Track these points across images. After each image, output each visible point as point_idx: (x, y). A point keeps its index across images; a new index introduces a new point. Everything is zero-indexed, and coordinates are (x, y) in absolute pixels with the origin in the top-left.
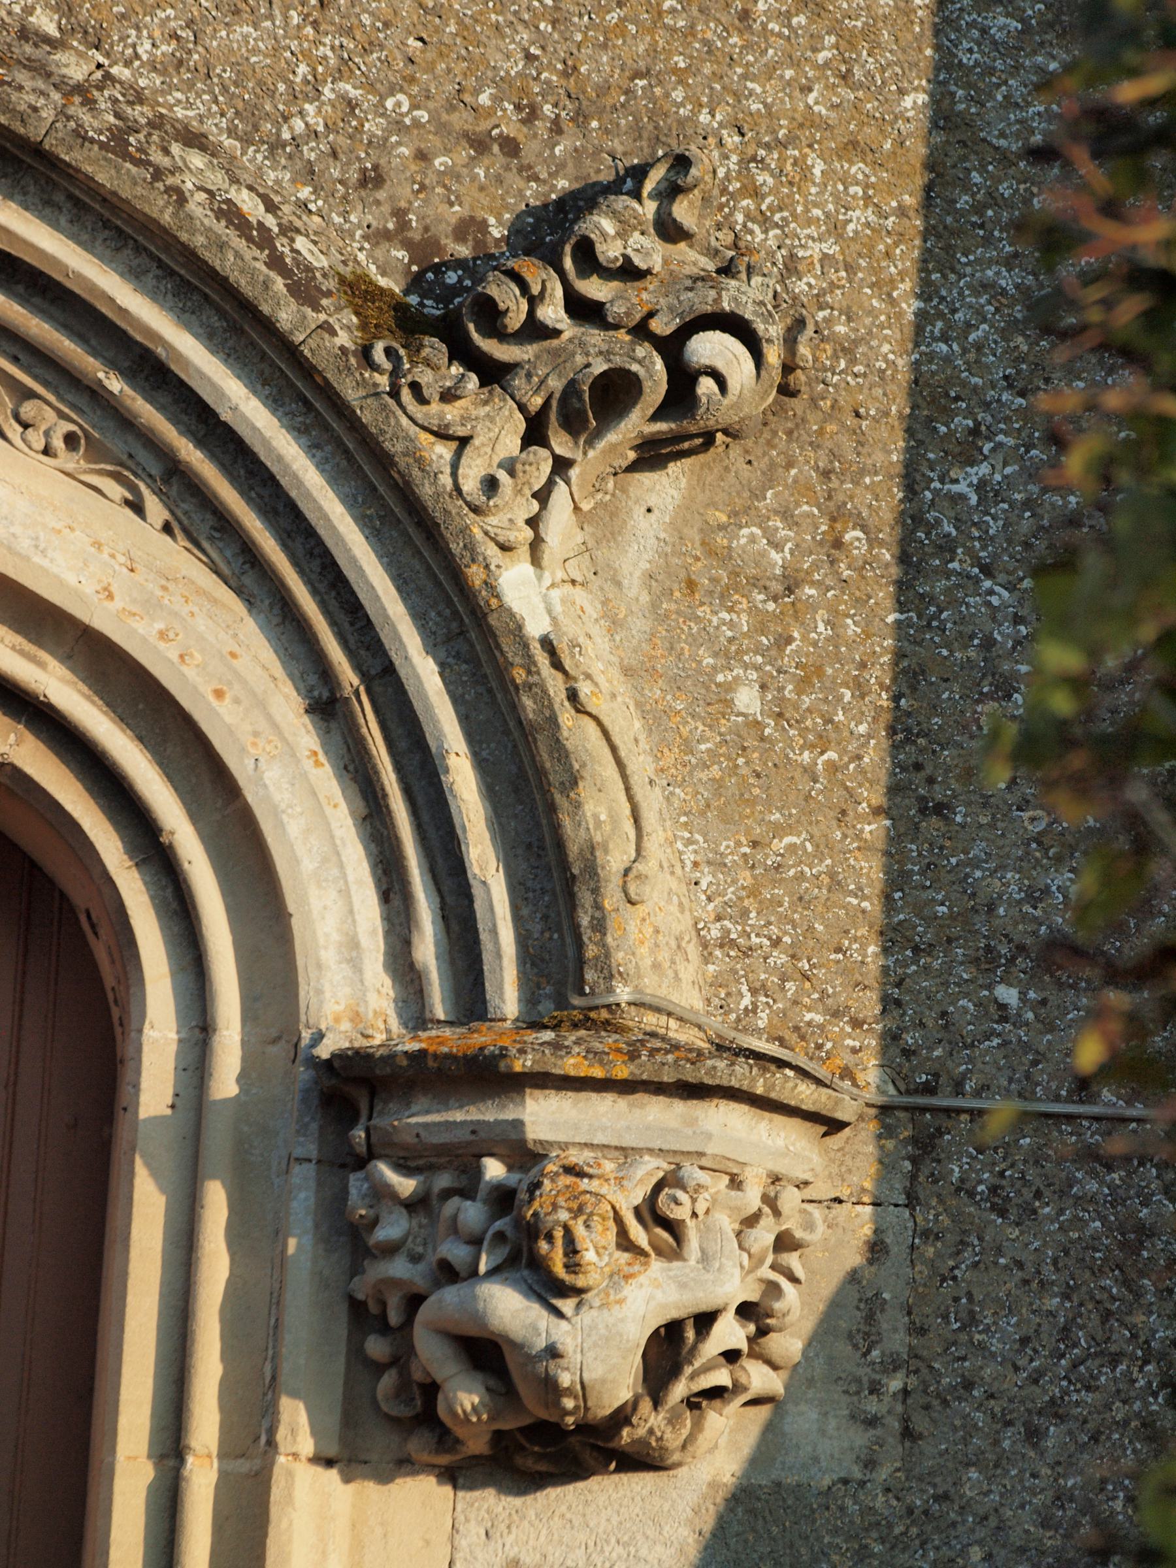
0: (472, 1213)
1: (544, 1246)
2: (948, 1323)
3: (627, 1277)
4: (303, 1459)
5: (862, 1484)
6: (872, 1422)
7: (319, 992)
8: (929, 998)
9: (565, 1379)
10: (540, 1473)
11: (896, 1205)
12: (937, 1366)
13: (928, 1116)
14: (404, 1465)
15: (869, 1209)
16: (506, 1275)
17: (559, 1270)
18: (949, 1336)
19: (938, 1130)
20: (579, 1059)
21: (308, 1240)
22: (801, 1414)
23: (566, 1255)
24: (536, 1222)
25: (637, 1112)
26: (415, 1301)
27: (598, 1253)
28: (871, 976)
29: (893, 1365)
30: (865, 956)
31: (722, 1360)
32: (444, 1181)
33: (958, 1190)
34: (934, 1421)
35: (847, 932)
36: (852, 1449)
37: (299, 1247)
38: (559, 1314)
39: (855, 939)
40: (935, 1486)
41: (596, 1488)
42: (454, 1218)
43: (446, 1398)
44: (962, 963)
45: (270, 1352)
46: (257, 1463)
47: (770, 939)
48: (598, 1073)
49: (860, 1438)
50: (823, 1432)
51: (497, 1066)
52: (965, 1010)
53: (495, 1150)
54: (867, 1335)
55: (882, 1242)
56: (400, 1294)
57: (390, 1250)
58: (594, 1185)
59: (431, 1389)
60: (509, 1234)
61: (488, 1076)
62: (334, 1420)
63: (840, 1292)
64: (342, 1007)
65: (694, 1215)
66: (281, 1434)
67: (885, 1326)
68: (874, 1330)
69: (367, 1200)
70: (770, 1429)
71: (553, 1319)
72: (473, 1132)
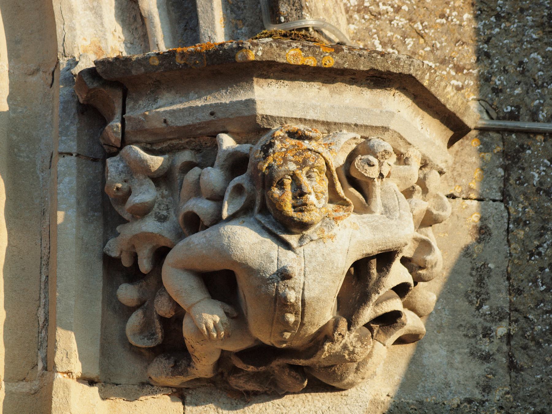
0: (213, 176)
1: (276, 192)
2: (537, 286)
3: (336, 219)
4: (75, 377)
5: (482, 403)
6: (486, 358)
7: (72, 29)
8: (509, 52)
9: (292, 296)
10: (248, 393)
11: (494, 201)
12: (531, 317)
13: (514, 136)
14: (147, 386)
15: (475, 203)
16: (241, 220)
17: (289, 210)
18: (538, 295)
19: (522, 146)
20: (298, 51)
21: (73, 213)
22: (435, 351)
23: (294, 198)
24: (271, 174)
25: (336, 97)
26: (160, 254)
27: (317, 197)
28: (467, 35)
29: (499, 316)
30: (462, 21)
31: (394, 293)
32: (186, 156)
33: (538, 190)
34: (531, 357)
35: (448, 3)
36: (473, 377)
37: (66, 218)
38: (287, 246)
39: (454, 8)
40: (534, 405)
41: (289, 403)
42: (197, 183)
43: (193, 320)
44: (531, 27)
45: (43, 301)
46: (36, 385)
47: (393, 7)
48: (311, 62)
49: (479, 369)
50: (451, 364)
51: (234, 57)
52: (536, 61)
53: (229, 128)
54: (478, 294)
55: (486, 227)
56: (149, 247)
57: (142, 212)
58: (313, 145)
59: (179, 314)
60: (245, 186)
61: (226, 67)
62: (95, 350)
63: (458, 262)
64: (88, 43)
65: (381, 176)
66: (59, 357)
67: (491, 288)
68: (483, 291)
69: (123, 176)
70: (414, 361)
71: (282, 250)
72: (212, 114)
